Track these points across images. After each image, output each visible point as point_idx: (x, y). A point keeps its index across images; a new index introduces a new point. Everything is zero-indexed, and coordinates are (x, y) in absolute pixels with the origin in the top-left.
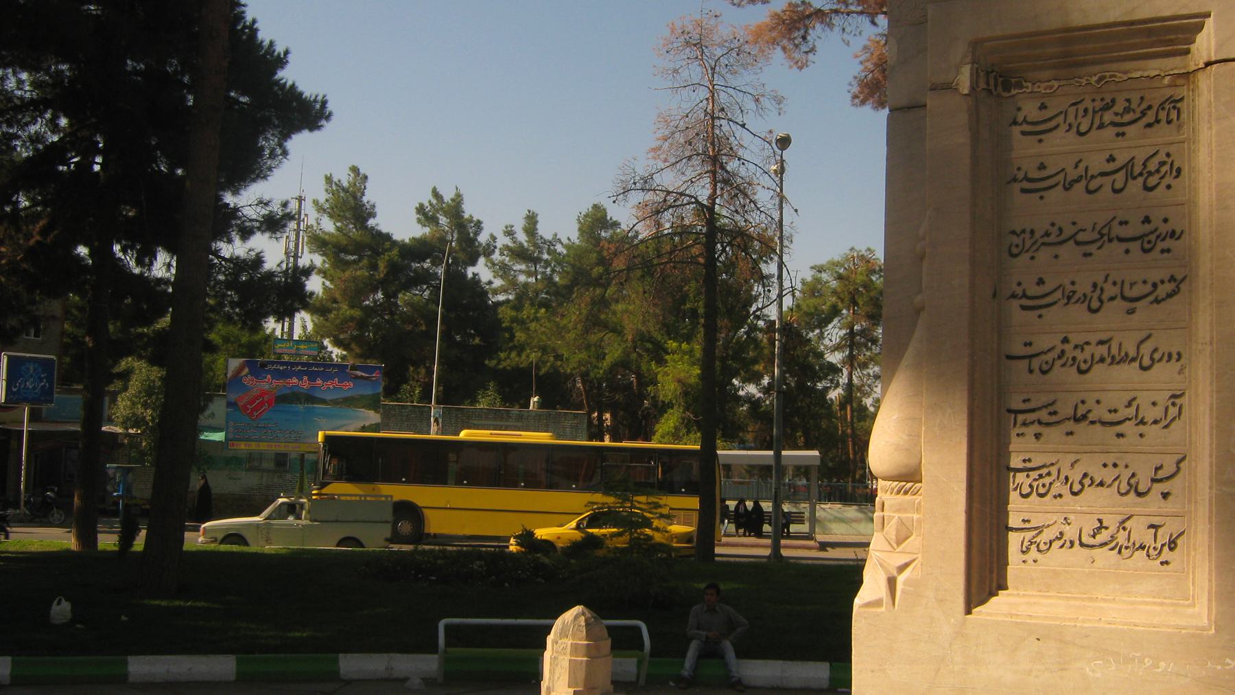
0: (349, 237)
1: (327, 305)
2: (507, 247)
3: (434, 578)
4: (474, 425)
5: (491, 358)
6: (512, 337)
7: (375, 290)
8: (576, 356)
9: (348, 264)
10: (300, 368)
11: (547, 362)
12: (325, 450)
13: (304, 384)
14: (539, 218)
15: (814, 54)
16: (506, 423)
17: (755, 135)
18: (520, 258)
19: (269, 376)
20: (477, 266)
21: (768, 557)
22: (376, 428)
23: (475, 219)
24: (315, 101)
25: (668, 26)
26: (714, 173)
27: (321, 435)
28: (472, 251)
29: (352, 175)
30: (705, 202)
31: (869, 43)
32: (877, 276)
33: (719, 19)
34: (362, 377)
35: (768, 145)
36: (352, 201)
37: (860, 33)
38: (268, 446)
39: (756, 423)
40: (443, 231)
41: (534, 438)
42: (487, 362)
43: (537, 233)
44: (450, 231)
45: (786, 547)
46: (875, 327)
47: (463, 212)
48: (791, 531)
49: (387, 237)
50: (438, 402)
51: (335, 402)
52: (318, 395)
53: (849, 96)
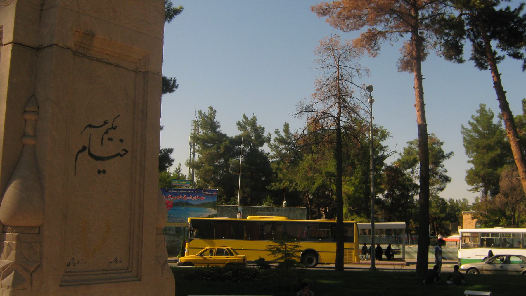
0: (209, 136)
1: (199, 165)
2: (276, 138)
3: (209, 278)
4: (259, 214)
5: (268, 186)
6: (277, 176)
7: (220, 158)
8: (303, 183)
9: (208, 147)
10: (183, 191)
11: (292, 186)
12: (191, 226)
13: (185, 198)
14: (290, 126)
15: (380, 50)
16: (272, 213)
17: (358, 86)
18: (282, 142)
19: (170, 195)
20: (263, 147)
21: (370, 269)
22: (214, 216)
23: (262, 127)
24: (171, 80)
25: (320, 42)
26: (339, 103)
27: (189, 219)
28: (261, 140)
29: (210, 110)
30: (336, 116)
31: (405, 45)
32: (437, 145)
33: (339, 38)
34: (209, 195)
35: (364, 90)
36: (210, 121)
37: (397, 41)
38: (177, 224)
39: (382, 211)
40: (249, 132)
41: (278, 219)
42: (266, 187)
43: (289, 132)
44: (251, 132)
45: (368, 264)
46: (436, 167)
47: (256, 124)
48: (394, 257)
49: (225, 136)
50: (240, 204)
51: (198, 205)
52: (191, 202)
53: (397, 67)
